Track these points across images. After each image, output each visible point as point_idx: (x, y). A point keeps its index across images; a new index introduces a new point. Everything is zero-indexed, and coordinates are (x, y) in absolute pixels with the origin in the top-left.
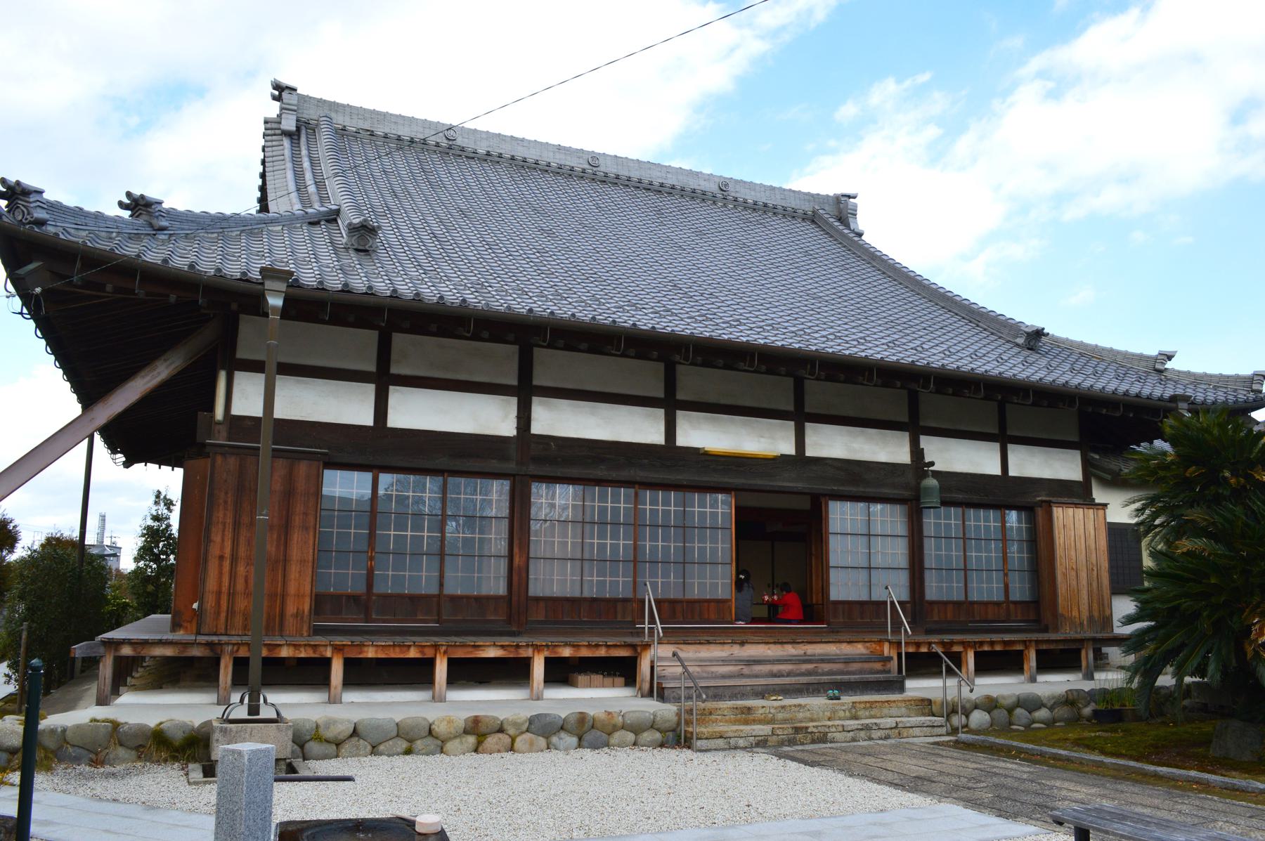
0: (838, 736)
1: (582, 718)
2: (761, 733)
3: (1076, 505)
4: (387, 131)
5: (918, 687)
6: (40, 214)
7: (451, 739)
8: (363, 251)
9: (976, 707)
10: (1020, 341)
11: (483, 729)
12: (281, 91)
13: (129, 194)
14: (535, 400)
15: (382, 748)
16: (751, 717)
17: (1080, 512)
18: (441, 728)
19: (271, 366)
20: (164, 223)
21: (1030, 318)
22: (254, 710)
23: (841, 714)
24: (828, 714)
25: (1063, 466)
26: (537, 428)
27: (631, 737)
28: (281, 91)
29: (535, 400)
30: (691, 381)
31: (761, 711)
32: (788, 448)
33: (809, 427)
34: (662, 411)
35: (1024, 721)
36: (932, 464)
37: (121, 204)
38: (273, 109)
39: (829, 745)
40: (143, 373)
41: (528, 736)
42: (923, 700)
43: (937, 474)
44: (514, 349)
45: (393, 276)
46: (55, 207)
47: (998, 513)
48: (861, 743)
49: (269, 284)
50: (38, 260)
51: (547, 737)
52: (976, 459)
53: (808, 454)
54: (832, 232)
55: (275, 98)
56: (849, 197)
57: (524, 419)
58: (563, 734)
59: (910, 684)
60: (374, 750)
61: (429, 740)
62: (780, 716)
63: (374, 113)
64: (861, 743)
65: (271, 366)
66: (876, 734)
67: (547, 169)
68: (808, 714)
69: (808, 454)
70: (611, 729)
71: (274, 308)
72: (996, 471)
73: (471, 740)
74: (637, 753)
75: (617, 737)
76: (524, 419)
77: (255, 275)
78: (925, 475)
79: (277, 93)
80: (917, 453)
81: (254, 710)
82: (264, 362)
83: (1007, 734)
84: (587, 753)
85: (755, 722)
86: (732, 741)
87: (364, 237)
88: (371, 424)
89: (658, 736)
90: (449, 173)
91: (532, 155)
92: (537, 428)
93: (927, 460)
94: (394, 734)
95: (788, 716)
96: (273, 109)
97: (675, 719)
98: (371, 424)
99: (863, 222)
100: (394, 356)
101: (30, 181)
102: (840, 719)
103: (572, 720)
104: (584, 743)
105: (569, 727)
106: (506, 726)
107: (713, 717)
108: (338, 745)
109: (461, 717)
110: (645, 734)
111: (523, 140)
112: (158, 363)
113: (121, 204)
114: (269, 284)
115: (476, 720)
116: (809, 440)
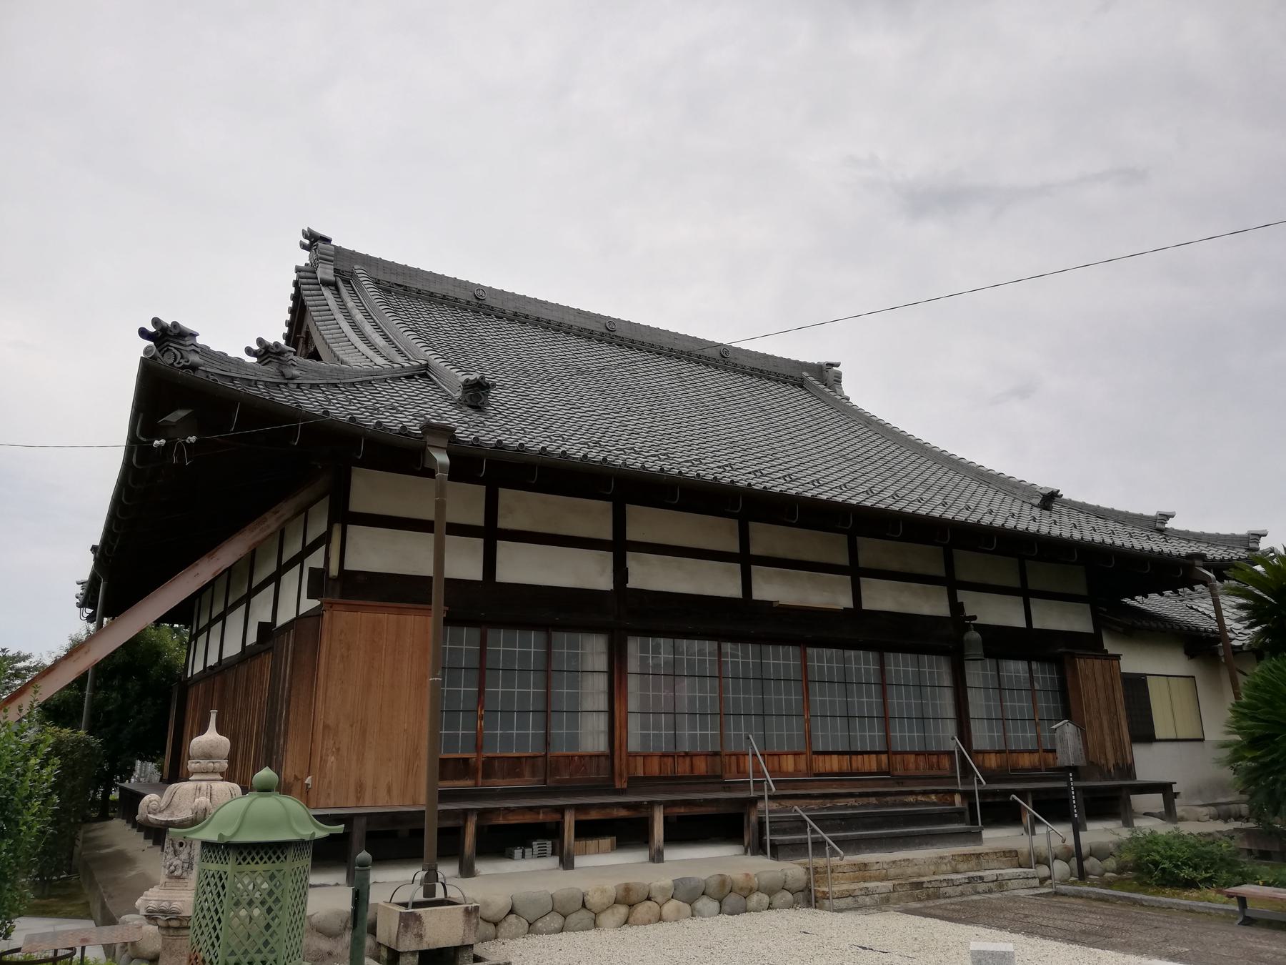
0: (950, 891)
1: (723, 881)
2: (884, 890)
3: (1089, 657)
4: (420, 287)
5: (996, 838)
6: (195, 358)
7: (603, 911)
8: (478, 408)
9: (1056, 858)
10: (1037, 501)
11: (633, 898)
12: (314, 241)
13: (260, 341)
14: (629, 555)
15: (539, 924)
16: (867, 874)
17: (1097, 662)
18: (595, 899)
19: (440, 527)
20: (296, 373)
21: (1044, 481)
22: (429, 891)
23: (944, 868)
24: (932, 868)
25: (1075, 620)
26: (632, 583)
27: (765, 899)
28: (314, 241)
29: (629, 555)
30: (872, 551)
31: (876, 867)
32: (845, 602)
33: (864, 581)
34: (611, 554)
35: (1098, 870)
36: (975, 618)
37: (249, 351)
38: (304, 258)
39: (942, 901)
40: (251, 525)
41: (674, 903)
42: (1010, 851)
43: (982, 629)
44: (608, 505)
45: (498, 429)
46: (205, 351)
47: (994, 661)
48: (970, 898)
49: (430, 440)
50: (182, 407)
51: (691, 902)
52: (1000, 612)
53: (864, 607)
54: (823, 398)
55: (304, 247)
56: (832, 365)
57: (620, 572)
58: (705, 900)
59: (988, 834)
60: (531, 928)
61: (584, 914)
62: (892, 872)
63: (405, 270)
64: (970, 898)
65: (440, 527)
66: (981, 887)
67: (568, 331)
68: (915, 869)
69: (864, 607)
70: (748, 892)
71: (442, 465)
72: (1021, 623)
73: (622, 910)
74: (772, 914)
75: (755, 899)
76: (620, 572)
77: (415, 428)
78: (966, 628)
79: (307, 242)
80: (956, 607)
81: (429, 891)
82: (432, 522)
83: (25, 658)
84: (724, 918)
85: (871, 879)
86: (860, 899)
87: (476, 395)
88: (480, 578)
89: (789, 896)
90: (487, 330)
91: (555, 317)
92: (632, 583)
93: (968, 614)
94: (550, 908)
95: (898, 871)
96: (304, 258)
97: (805, 878)
98: (480, 578)
99: (849, 388)
100: (500, 512)
101: (187, 324)
102: (944, 873)
103: (714, 883)
104: (726, 908)
105: (710, 891)
106: (653, 894)
107: (835, 875)
108: (496, 924)
109: (611, 886)
110: (779, 896)
111: (546, 303)
112: (267, 515)
113: (249, 351)
114: (430, 440)
115: (627, 889)
116: (865, 594)
